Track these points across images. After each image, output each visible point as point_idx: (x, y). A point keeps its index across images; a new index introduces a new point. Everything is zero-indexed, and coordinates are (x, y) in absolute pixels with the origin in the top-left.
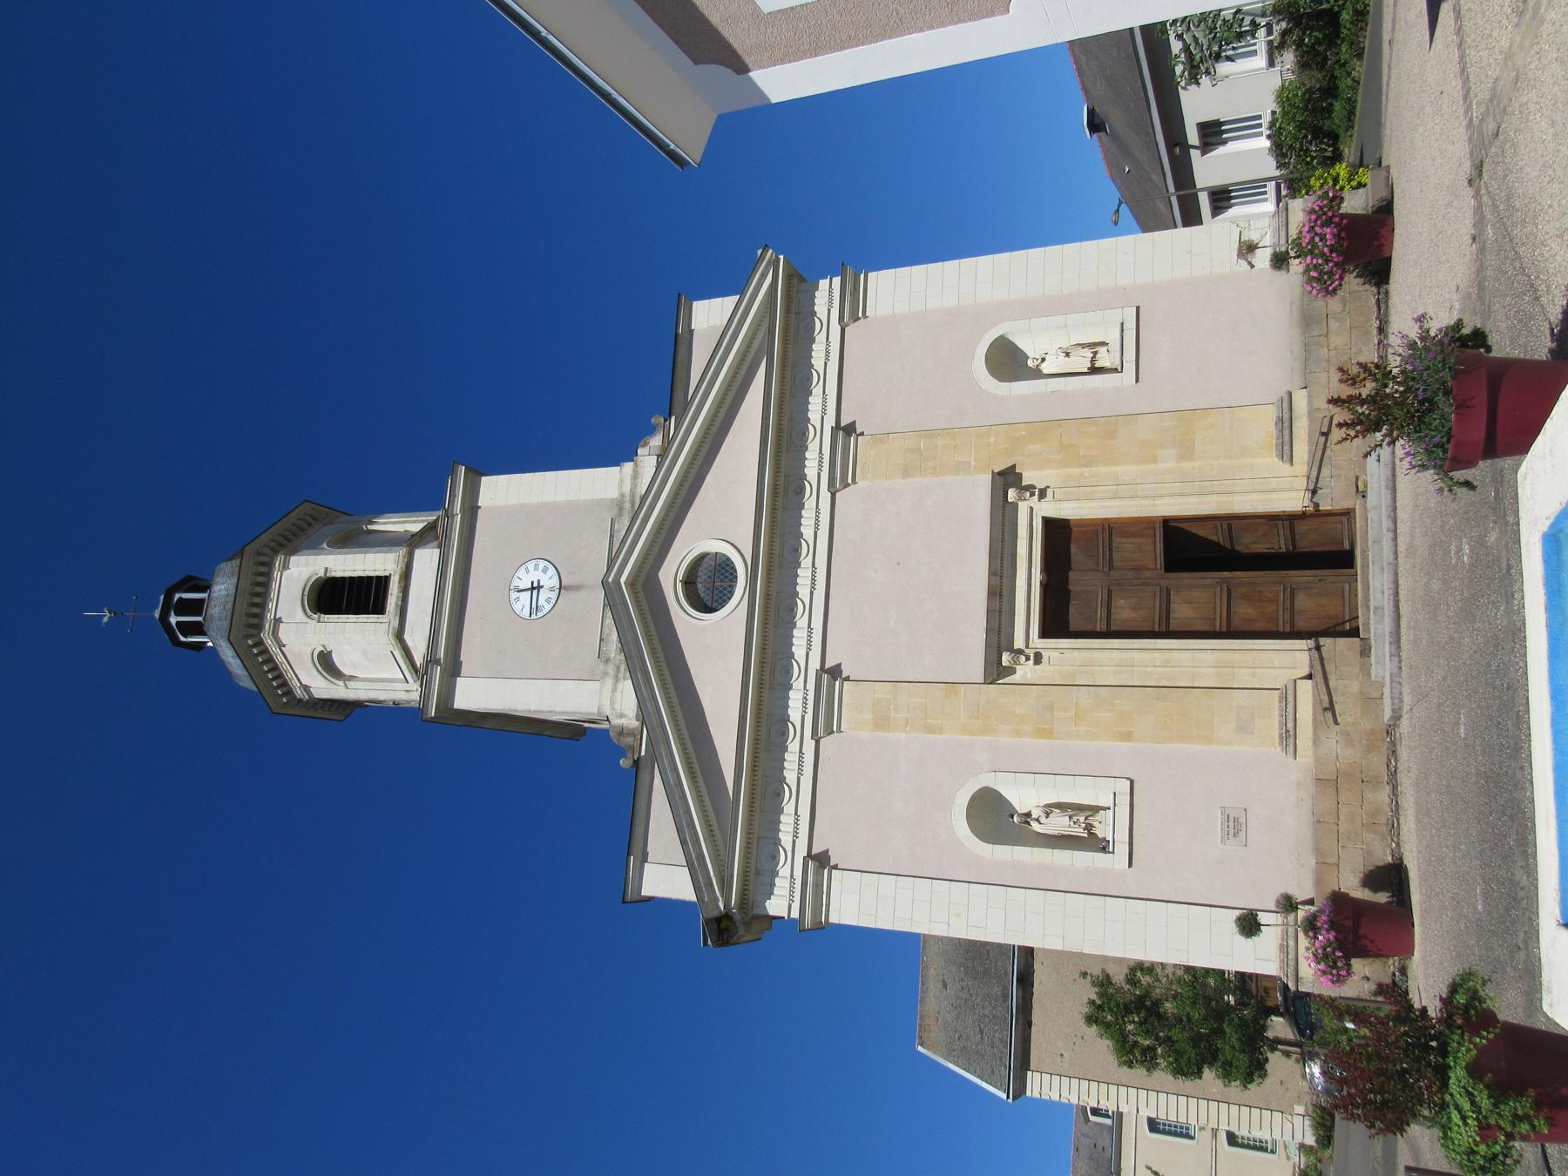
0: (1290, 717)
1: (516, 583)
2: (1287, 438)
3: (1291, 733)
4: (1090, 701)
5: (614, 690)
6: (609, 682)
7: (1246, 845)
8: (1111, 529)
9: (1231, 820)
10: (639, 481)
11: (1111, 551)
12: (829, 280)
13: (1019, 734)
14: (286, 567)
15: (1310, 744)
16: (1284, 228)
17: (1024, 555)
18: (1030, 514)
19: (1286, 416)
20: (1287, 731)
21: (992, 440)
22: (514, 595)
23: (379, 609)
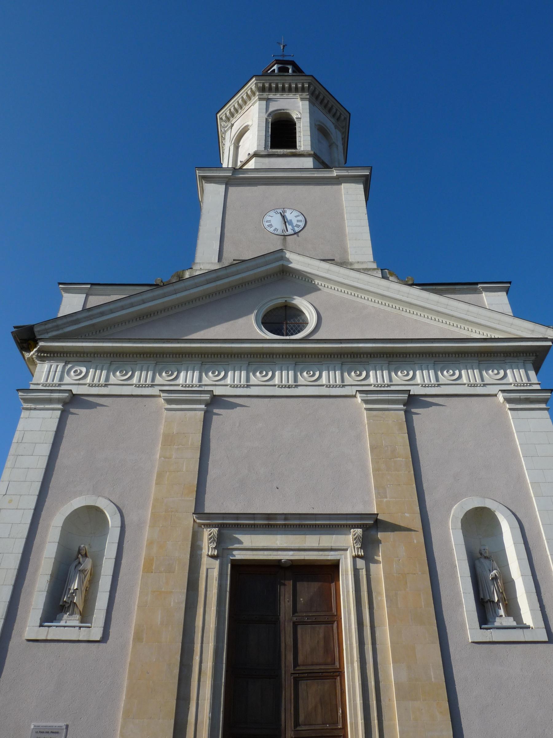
8: (332, 623)
11: (312, 623)
12: (537, 382)
13: (150, 543)
14: (302, 99)
17: (304, 545)
21: (407, 515)
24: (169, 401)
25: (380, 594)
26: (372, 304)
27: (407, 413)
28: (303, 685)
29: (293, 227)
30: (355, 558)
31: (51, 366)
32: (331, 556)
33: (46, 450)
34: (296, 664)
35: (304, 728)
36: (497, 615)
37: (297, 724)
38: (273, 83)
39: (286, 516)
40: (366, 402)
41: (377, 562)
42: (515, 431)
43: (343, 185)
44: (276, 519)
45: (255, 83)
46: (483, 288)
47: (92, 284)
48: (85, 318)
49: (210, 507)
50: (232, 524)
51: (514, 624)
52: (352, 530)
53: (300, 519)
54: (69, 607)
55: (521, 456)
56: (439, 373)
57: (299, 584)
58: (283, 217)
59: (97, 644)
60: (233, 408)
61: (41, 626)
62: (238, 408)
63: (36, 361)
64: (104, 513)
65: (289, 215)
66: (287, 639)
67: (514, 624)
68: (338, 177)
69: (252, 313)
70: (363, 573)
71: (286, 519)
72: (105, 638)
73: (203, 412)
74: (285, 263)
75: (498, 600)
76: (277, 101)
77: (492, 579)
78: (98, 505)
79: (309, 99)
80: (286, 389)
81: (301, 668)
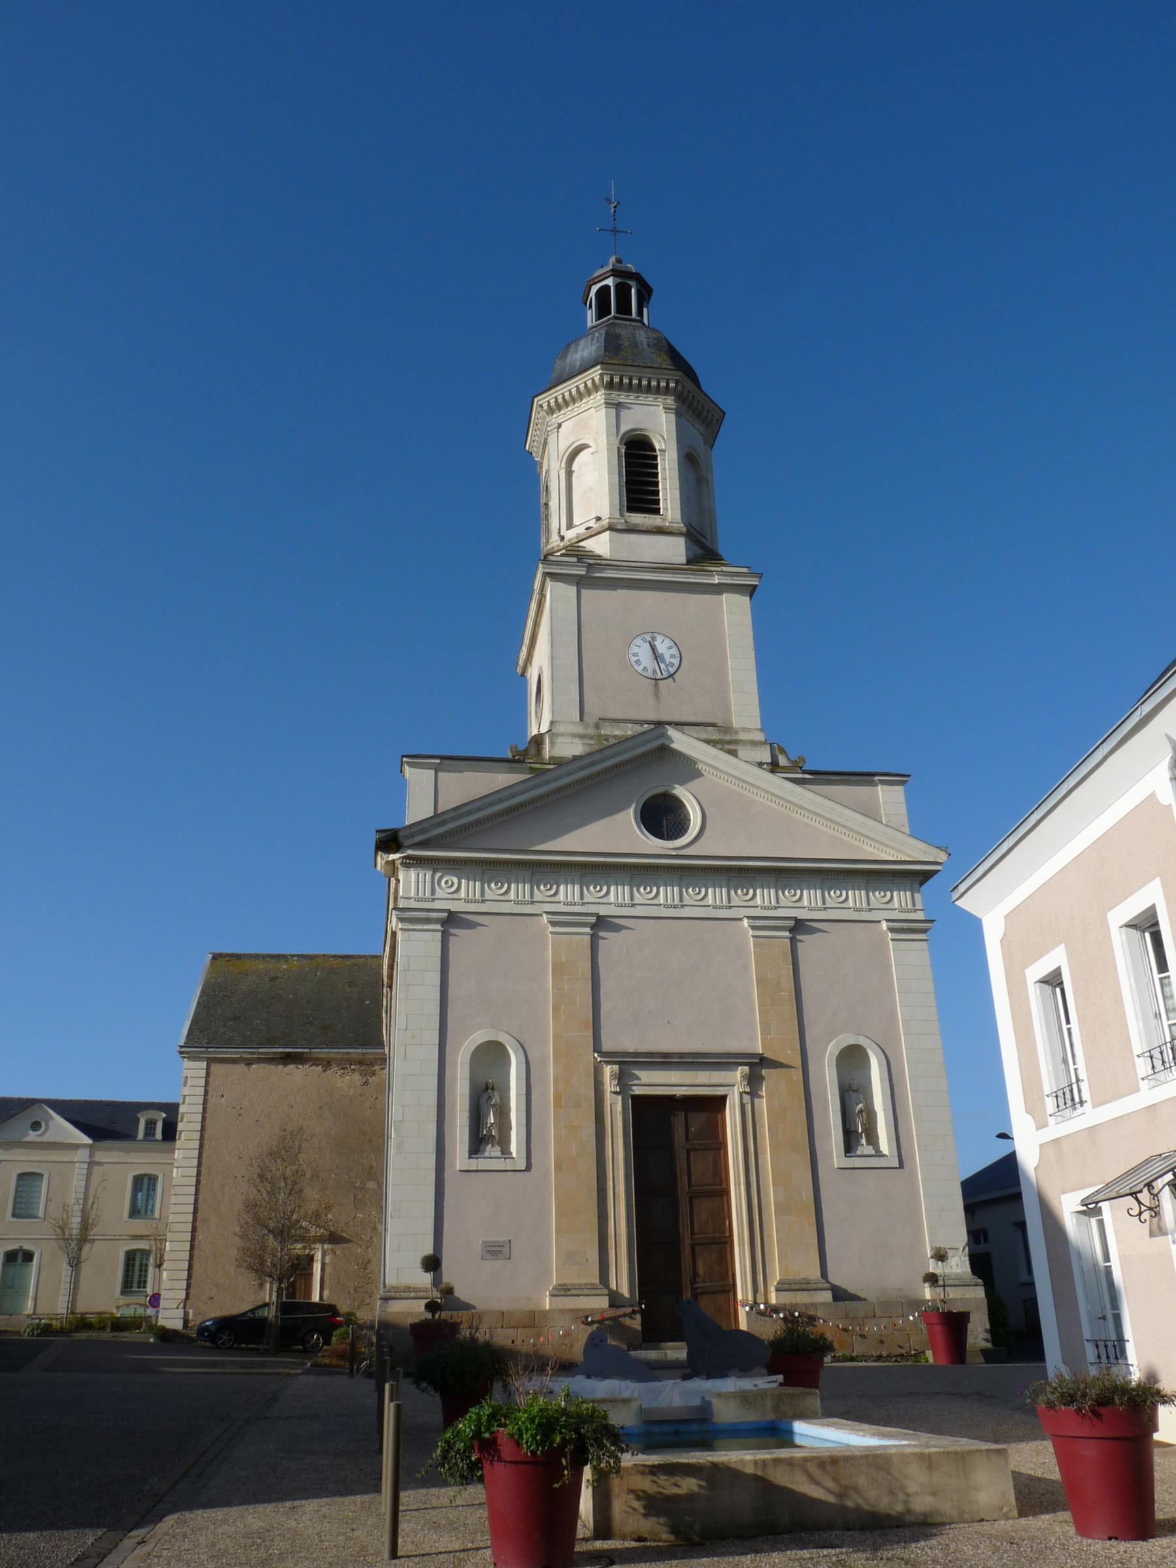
0: (580, 1292)
1: (659, 639)
2: (794, 1287)
3: (568, 1293)
4: (584, 1137)
5: (574, 735)
6: (580, 730)
7: (510, 1258)
9: (501, 1249)
10: (749, 748)
11: (702, 1150)
15: (560, 1307)
16: (961, 1283)
18: (733, 1083)
19: (811, 1286)
20: (569, 1290)
21: (789, 1052)
22: (648, 638)
23: (632, 508)
24: (553, 924)
25: (763, 1126)
26: (761, 800)
27: (793, 941)
28: (696, 1203)
29: (667, 666)
30: (741, 1094)
31: (418, 874)
32: (720, 1091)
33: (435, 978)
34: (690, 1185)
35: (698, 1236)
36: (859, 1144)
37: (692, 1233)
38: (626, 375)
39: (681, 1055)
40: (753, 928)
41: (761, 1097)
42: (893, 964)
43: (724, 596)
44: (673, 1058)
45: (601, 374)
46: (879, 780)
47: (442, 758)
48: (451, 818)
49: (607, 1046)
50: (633, 1062)
51: (873, 1152)
52: (740, 1068)
53: (692, 1058)
54: (488, 1140)
55: (896, 991)
56: (826, 893)
57: (690, 1115)
58: (653, 649)
59: (522, 1173)
60: (618, 931)
61: (470, 1158)
62: (624, 931)
63: (400, 867)
64: (505, 1047)
65: (662, 646)
66: (681, 1164)
67: (873, 1152)
68: (719, 585)
69: (630, 807)
70: (749, 1107)
71: (680, 1058)
72: (528, 1168)
73: (589, 937)
74: (667, 742)
75: (862, 1132)
76: (630, 408)
77: (859, 1112)
78: (499, 1040)
79: (676, 409)
80: (672, 909)
81: (694, 1188)
